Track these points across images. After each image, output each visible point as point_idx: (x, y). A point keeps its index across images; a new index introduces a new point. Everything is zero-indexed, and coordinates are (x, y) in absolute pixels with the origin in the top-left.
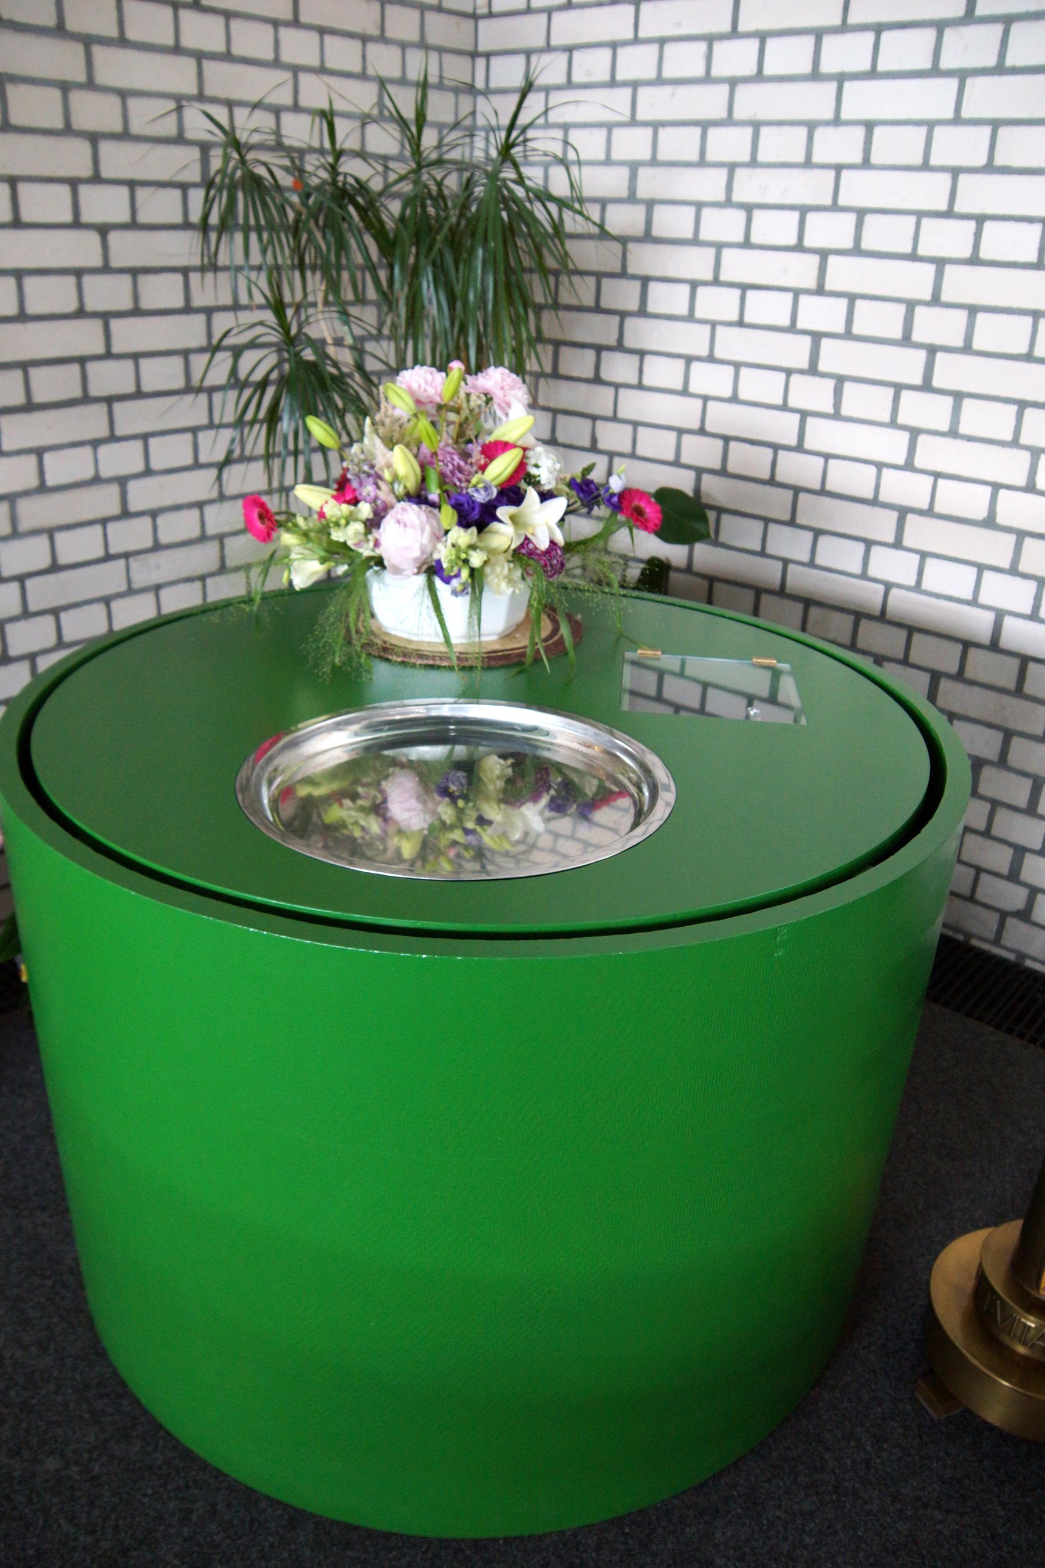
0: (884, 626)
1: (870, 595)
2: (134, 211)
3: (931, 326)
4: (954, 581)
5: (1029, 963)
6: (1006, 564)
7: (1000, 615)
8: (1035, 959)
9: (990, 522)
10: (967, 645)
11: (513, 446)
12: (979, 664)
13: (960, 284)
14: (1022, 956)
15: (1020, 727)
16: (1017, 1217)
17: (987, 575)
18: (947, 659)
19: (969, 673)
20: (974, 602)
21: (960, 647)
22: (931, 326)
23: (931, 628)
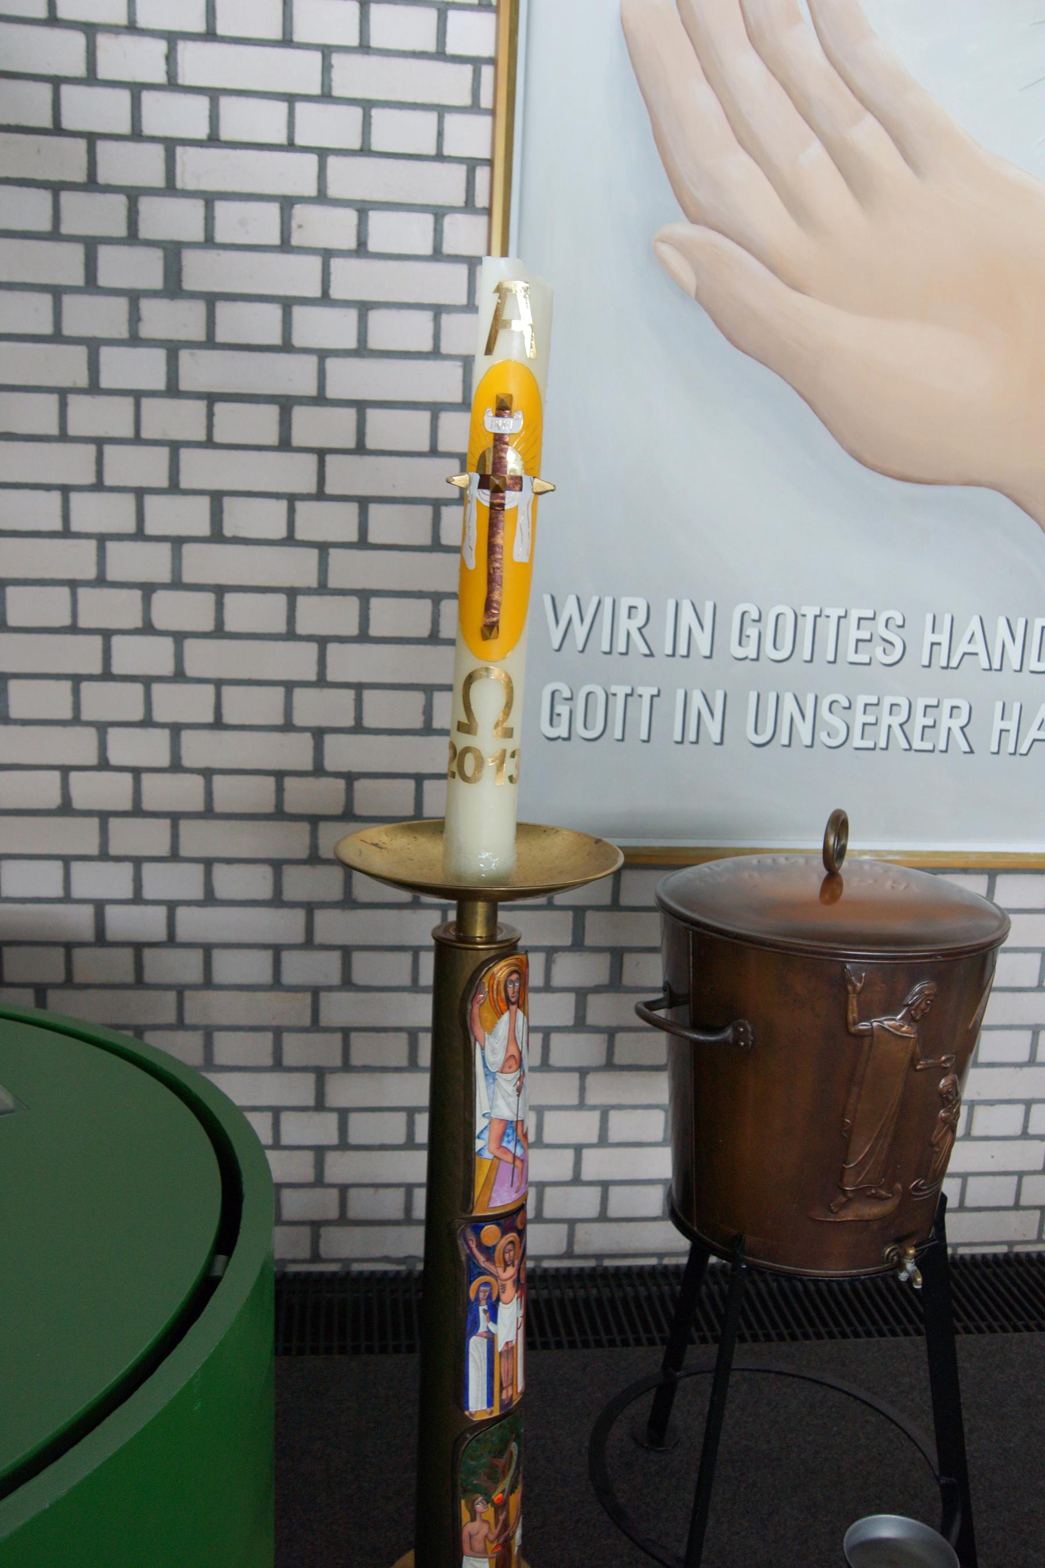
0: (176, 950)
1: (79, 920)
2: (210, 415)
3: (317, 615)
4: (45, 880)
5: (356, 1267)
6: (94, 850)
7: (100, 906)
8: (294, 1261)
9: (66, 809)
10: (69, 947)
11: (555, 831)
12: (89, 964)
13: (347, 570)
14: (347, 1261)
15: (149, 1020)
16: (409, 1550)
17: (76, 867)
18: (49, 967)
19: (79, 977)
20: (67, 898)
21: (62, 950)
22: (317, 615)
23: (26, 938)
